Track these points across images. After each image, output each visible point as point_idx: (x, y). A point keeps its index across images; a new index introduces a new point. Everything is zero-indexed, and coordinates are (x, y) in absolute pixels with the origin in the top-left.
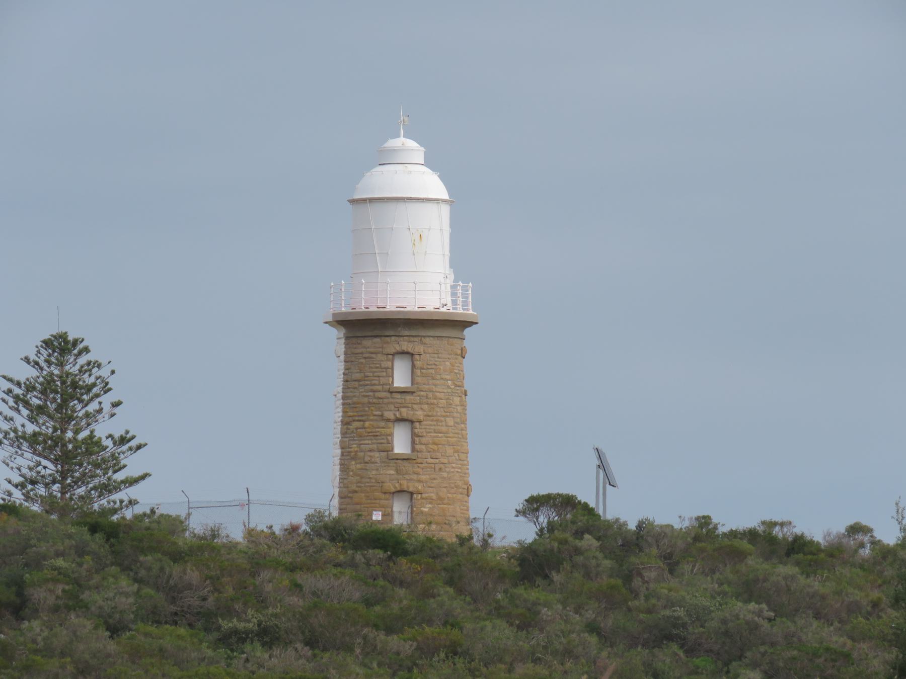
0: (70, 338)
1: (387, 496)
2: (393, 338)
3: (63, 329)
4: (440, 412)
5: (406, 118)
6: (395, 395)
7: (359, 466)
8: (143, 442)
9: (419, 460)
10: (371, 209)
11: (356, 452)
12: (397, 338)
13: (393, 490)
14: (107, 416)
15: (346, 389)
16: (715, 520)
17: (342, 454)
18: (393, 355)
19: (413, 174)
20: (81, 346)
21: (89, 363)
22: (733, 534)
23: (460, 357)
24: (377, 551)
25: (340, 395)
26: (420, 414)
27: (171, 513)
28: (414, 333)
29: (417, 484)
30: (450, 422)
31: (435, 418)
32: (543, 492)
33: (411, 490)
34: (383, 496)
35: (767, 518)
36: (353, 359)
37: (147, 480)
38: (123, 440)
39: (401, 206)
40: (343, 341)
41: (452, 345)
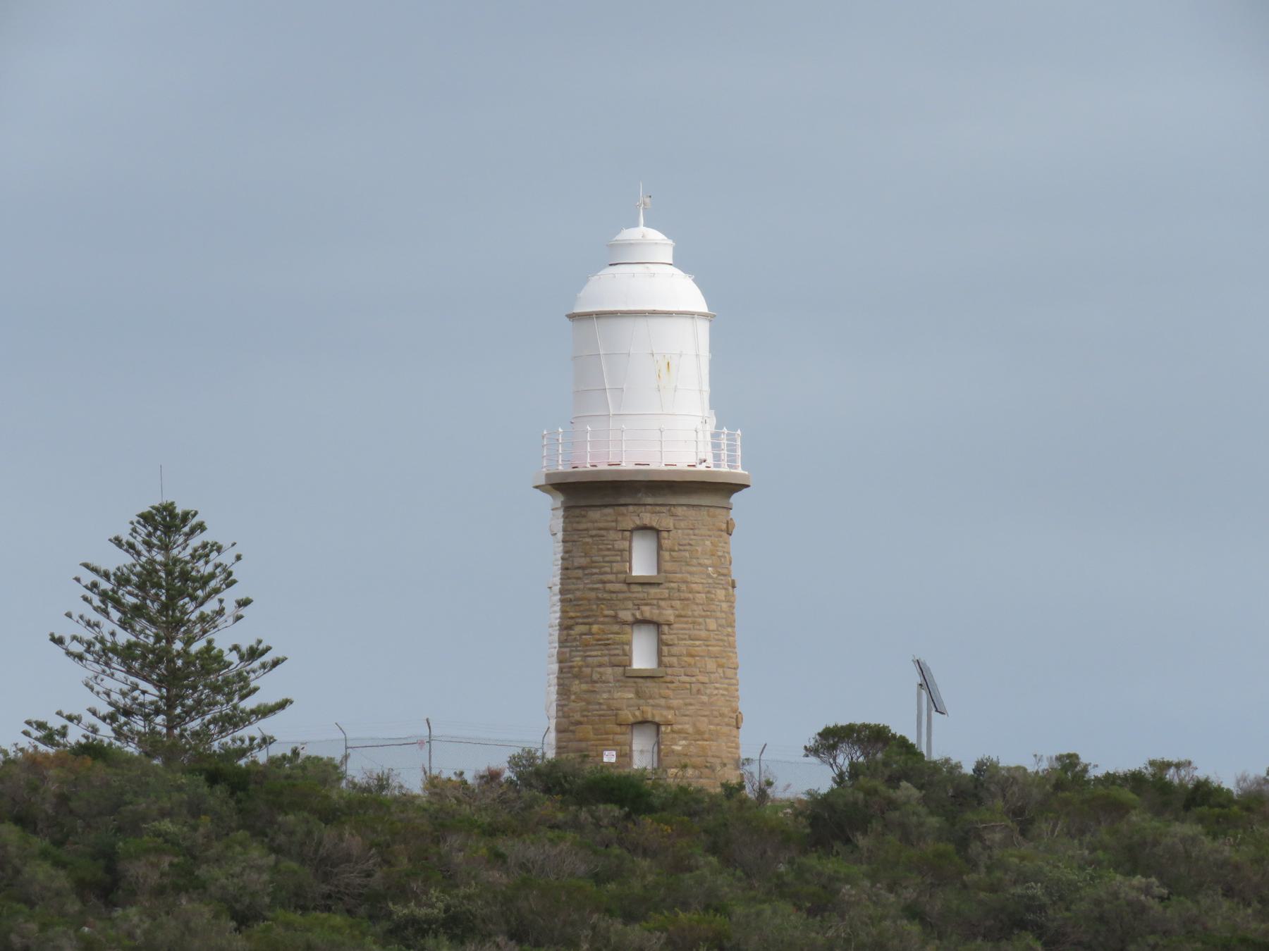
0: (179, 510)
1: (624, 729)
2: (631, 508)
3: (167, 499)
4: (698, 611)
5: (648, 200)
6: (635, 588)
7: (584, 687)
8: (281, 656)
9: (669, 678)
10: (597, 324)
11: (580, 667)
13: (632, 719)
14: (231, 620)
15: (565, 579)
16: (1084, 759)
17: (561, 670)
18: (631, 531)
19: (656, 277)
20: (194, 521)
21: (204, 546)
22: (1110, 779)
23: (725, 534)
24: (609, 807)
25: (557, 589)
26: (669, 614)
27: (1008, 758)
28: (660, 500)
29: (665, 712)
32: (843, 722)
33: (657, 719)
34: (618, 729)
35: (1158, 757)
36: (575, 537)
37: (289, 708)
38: (254, 653)
39: (641, 323)
40: (561, 513)
41: (714, 516)
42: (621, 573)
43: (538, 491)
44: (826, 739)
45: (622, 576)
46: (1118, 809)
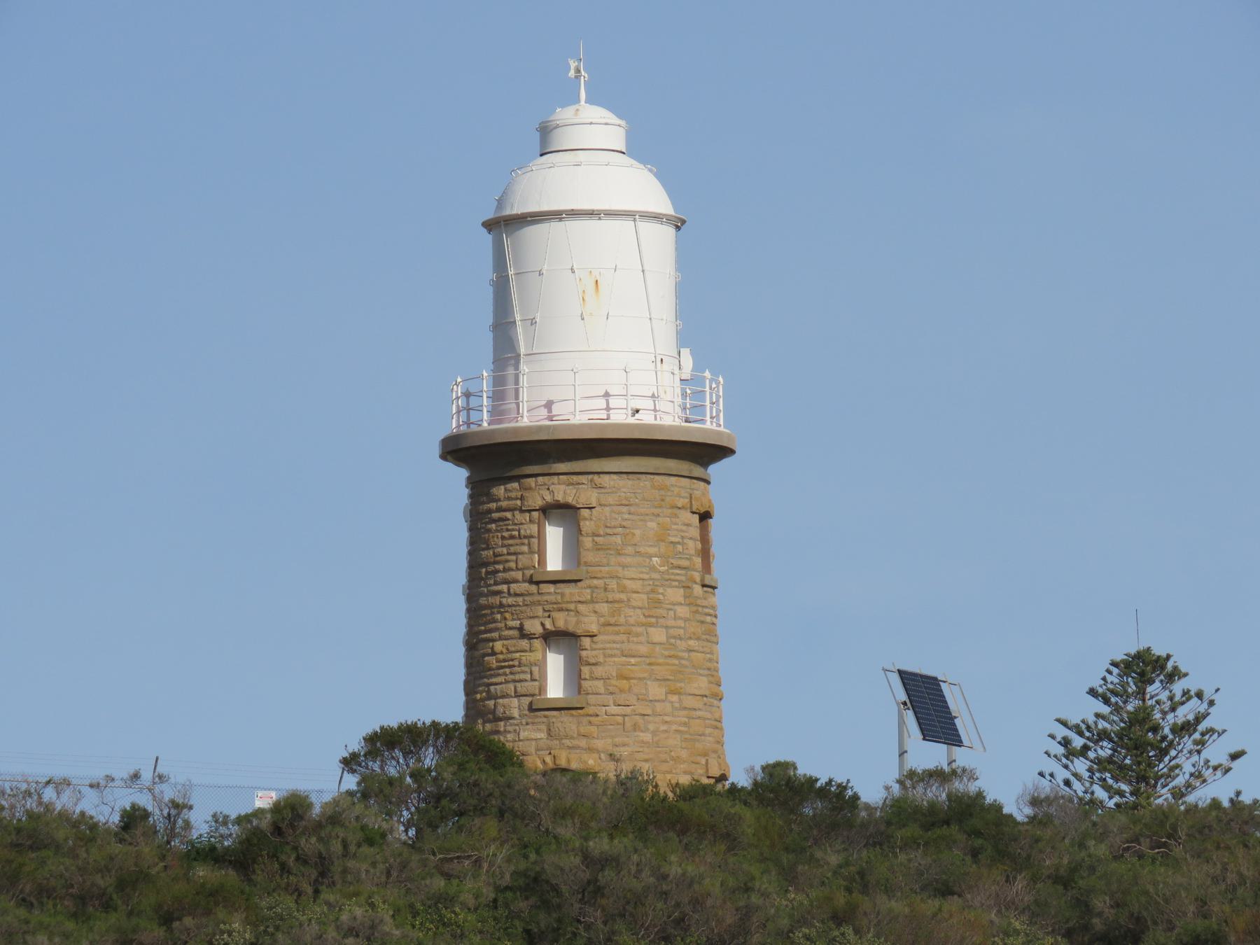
2: (540, 479)
4: (634, 616)
8: (1218, 728)
9: (591, 710)
19: (597, 171)
29: (585, 756)
30: (658, 635)
42: (527, 568)
45: (528, 573)
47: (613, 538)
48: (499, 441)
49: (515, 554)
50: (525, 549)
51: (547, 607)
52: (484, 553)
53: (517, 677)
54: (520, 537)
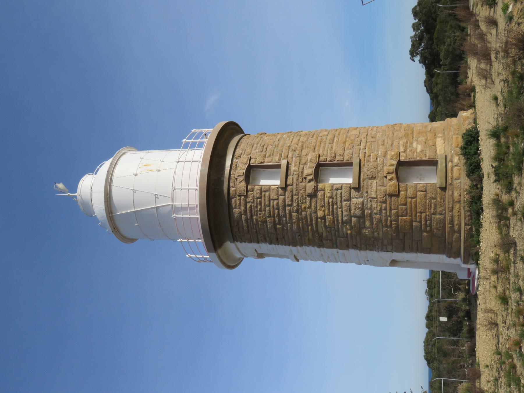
2: (231, 185)
9: (361, 156)
12: (232, 181)
17: (355, 247)
31: (318, 144)
42: (278, 192)
43: (136, 238)
44: (418, 29)
46: (430, 286)
47: (268, 149)
48: (206, 213)
49: (269, 201)
50: (267, 193)
51: (300, 180)
52: (269, 225)
53: (339, 199)
54: (261, 198)
